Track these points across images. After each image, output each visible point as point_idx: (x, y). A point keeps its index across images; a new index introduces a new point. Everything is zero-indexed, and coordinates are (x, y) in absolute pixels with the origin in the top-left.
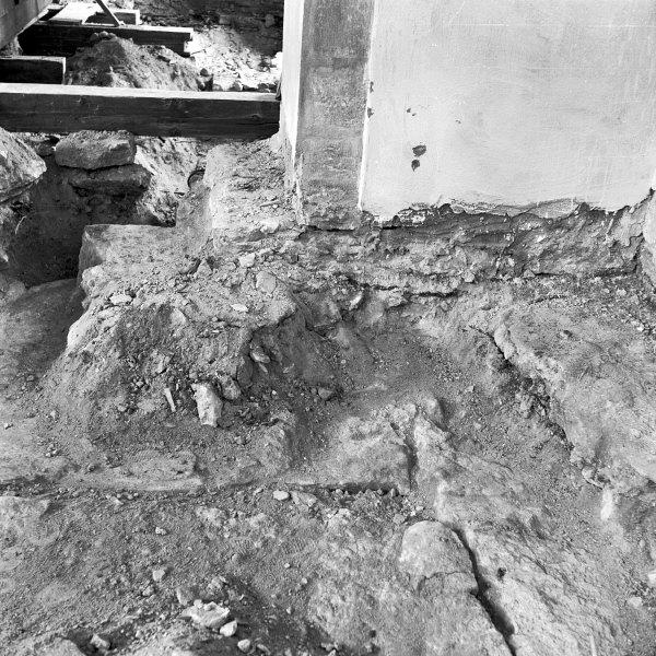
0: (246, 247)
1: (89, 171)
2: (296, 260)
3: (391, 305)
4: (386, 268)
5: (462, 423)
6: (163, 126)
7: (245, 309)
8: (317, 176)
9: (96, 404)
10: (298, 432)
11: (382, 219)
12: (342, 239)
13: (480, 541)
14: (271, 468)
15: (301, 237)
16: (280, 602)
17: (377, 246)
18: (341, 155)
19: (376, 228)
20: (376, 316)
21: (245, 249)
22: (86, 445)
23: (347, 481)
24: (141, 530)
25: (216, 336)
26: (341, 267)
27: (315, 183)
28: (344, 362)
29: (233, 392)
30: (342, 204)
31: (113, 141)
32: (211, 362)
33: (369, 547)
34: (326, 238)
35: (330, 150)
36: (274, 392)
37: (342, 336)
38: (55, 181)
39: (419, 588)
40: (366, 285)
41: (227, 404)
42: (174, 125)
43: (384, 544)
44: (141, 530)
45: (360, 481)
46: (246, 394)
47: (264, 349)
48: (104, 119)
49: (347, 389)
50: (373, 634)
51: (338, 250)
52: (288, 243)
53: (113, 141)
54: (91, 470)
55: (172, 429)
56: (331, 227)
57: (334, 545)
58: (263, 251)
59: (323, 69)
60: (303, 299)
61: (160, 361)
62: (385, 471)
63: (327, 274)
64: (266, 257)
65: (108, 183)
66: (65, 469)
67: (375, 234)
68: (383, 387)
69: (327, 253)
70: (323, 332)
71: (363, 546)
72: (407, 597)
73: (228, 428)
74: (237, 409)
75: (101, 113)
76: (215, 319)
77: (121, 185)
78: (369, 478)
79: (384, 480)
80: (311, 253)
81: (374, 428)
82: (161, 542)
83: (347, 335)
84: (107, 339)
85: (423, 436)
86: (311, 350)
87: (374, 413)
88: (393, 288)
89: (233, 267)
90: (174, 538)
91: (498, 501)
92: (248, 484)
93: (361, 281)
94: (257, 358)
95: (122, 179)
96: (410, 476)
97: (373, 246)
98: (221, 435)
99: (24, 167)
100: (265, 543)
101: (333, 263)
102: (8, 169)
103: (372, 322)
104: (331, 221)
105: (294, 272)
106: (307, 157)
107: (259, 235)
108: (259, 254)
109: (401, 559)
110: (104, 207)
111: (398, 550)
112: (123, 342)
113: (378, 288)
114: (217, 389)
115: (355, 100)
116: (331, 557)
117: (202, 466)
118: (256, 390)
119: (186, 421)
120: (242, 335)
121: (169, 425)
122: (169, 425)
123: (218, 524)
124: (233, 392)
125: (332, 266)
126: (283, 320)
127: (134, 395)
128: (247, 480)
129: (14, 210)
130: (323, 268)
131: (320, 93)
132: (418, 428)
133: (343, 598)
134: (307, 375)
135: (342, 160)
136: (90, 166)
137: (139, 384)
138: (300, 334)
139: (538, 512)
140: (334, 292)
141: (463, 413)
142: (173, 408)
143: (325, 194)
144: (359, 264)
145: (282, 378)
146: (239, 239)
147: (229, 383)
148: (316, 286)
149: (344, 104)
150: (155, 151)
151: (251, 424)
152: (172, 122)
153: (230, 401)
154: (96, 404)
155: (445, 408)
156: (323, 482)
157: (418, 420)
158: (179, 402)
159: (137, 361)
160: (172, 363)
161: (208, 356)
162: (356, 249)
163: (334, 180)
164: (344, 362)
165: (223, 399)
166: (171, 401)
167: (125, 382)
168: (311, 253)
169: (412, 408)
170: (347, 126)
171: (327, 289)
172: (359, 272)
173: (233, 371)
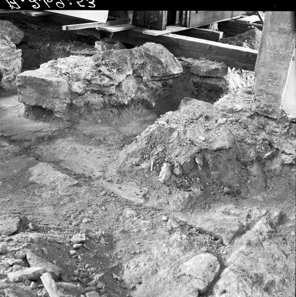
0: (225, 115)
1: (201, 77)
2: (246, 128)
3: (286, 162)
4: (291, 144)
5: (286, 229)
6: (240, 64)
7: (204, 139)
8: (262, 87)
9: (127, 158)
11: (290, 117)
12: (271, 122)
13: (228, 274)
14: (172, 207)
15: (251, 117)
16: (119, 253)
17: (288, 130)
18: (276, 79)
19: (287, 121)
20: (276, 165)
21: (224, 116)
22: (114, 172)
23: (200, 226)
24: (97, 205)
25: (184, 146)
26: (267, 137)
27: (261, 90)
28: (249, 181)
29: (177, 171)
30: (273, 104)
31: (215, 66)
32: (176, 156)
33: (177, 253)
34: (262, 120)
35: (271, 75)
36: (198, 179)
37: (254, 169)
38: (187, 78)
39: (178, 277)
40: (278, 149)
41: (174, 176)
42: (246, 64)
43: (184, 255)
44: (97, 205)
45: (206, 229)
46: (184, 174)
47: (204, 159)
48: (217, 56)
49: (243, 194)
50: (140, 283)
51: (267, 128)
52: (244, 118)
53: (215, 66)
54: (108, 181)
55: (145, 179)
56: (265, 115)
58: (231, 119)
59: (274, 33)
60: (241, 146)
61: (160, 149)
62: (222, 230)
63: (259, 138)
64: (232, 122)
65: (207, 84)
66: (100, 177)
67: (287, 124)
68: (261, 200)
69: (262, 128)
70: (245, 164)
72: (170, 278)
73: (168, 186)
74: (177, 179)
75: (216, 54)
76: (188, 139)
77: (212, 86)
78: (211, 229)
79: (218, 234)
80: (254, 125)
81: (237, 213)
82: (100, 212)
83: (257, 170)
84: (146, 135)
85: (261, 226)
87: (245, 208)
88: (291, 154)
89: (214, 122)
90: (106, 213)
91: (262, 266)
92: (159, 210)
93: (276, 146)
94: (197, 161)
95: (213, 83)
96: (234, 238)
97: (286, 130)
98: (164, 186)
99: (170, 68)
100: (139, 231)
101: (264, 133)
102: (163, 67)
103: (273, 167)
104: (265, 112)
105: (242, 133)
106: (259, 77)
107: (232, 111)
108: (229, 119)
109: (185, 264)
110: (203, 94)
111: (187, 260)
112: (150, 139)
113: (283, 152)
114: (172, 168)
115: (288, 51)
116: (159, 249)
117: (148, 196)
118: (191, 175)
119: (154, 177)
120: (195, 149)
121: (147, 176)
122: (147, 176)
123: (128, 217)
124: (177, 171)
125: (263, 135)
126: (219, 150)
127: (143, 159)
128: (159, 208)
129: (163, 85)
130: (258, 135)
131: (270, 45)
132: (260, 222)
134: (225, 180)
136: (201, 74)
137: (147, 156)
138: (229, 160)
139: (277, 279)
140: (257, 147)
141: (290, 224)
142: (151, 170)
143: (265, 97)
144: (277, 138)
145: (209, 176)
146: (223, 111)
147: (177, 167)
148: (249, 141)
149: (281, 53)
150: (247, 79)
151: (178, 188)
152: (244, 62)
153: (175, 175)
154: (127, 158)
155: (282, 218)
156: (190, 223)
157: (263, 218)
158: (155, 168)
159: (151, 147)
160: (162, 152)
161: (176, 154)
162: (277, 130)
163: (271, 91)
164: (249, 181)
165: (172, 172)
166: (152, 166)
167: (142, 154)
168: (254, 125)
169: (264, 212)
170: (281, 64)
171: (255, 144)
172: (276, 142)
173: (182, 163)
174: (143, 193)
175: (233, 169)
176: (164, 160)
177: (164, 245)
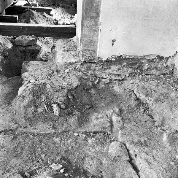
0: (67, 67)
1: (24, 47)
2: (80, 70)
3: (106, 83)
4: (105, 73)
5: (125, 115)
6: (44, 34)
7: (66, 84)
8: (86, 48)
9: (26, 110)
10: (81, 117)
11: (104, 59)
12: (93, 65)
13: (130, 147)
14: (74, 127)
15: (82, 64)
16: (76, 163)
17: (102, 67)
18: (93, 42)
19: (102, 62)
20: (102, 86)
21: (67, 68)
23: (94, 130)
24: (38, 144)
25: (59, 91)
26: (92, 73)
27: (86, 50)
28: (93, 98)
29: (63, 106)
30: (93, 55)
31: (31, 38)
32: (57, 98)
33: (100, 148)
34: (88, 65)
35: (90, 41)
36: (74, 106)
37: (93, 91)
38: (15, 49)
39: (114, 160)
40: (99, 77)
41: (62, 110)
42: (47, 34)
44: (38, 144)
45: (98, 130)
46: (67, 107)
47: (72, 95)
48: (28, 32)
49: (94, 106)
50: (101, 172)
51: (92, 68)
52: (78, 66)
53: (31, 38)
54: (25, 128)
55: (47, 116)
56: (90, 62)
58: (71, 68)
59: (88, 19)
60: (82, 81)
61: (43, 98)
62: (105, 128)
63: (89, 74)
64: (72, 70)
65: (29, 50)
66: (18, 127)
67: (102, 64)
68: (104, 105)
69: (89, 69)
70: (88, 90)
71: (99, 148)
72: (110, 162)
73: (62, 116)
74: (64, 111)
75: (28, 31)
76: (58, 87)
77: (33, 50)
78: (100, 130)
79: (104, 130)
80: (84, 69)
81: (102, 116)
82: (44, 147)
83: (94, 91)
85: (115, 118)
87: (101, 112)
88: (107, 78)
89: (63, 72)
91: (135, 136)
92: (67, 131)
93: (98, 76)
94: (70, 97)
95: (33, 49)
97: (101, 67)
98: (60, 118)
100: (72, 147)
101: (90, 71)
102: (2, 46)
103: (101, 87)
104: (90, 60)
105: (80, 74)
106: (83, 43)
107: (70, 64)
108: (70, 69)
109: (109, 152)
110: (28, 56)
111: (108, 149)
112: (34, 93)
113: (102, 78)
114: (59, 106)
115: (96, 27)
116: (90, 151)
117: (55, 127)
118: (70, 106)
119: (50, 114)
120: (66, 91)
121: (46, 115)
122: (46, 115)
123: (59, 142)
124: (63, 106)
125: (90, 72)
126: (77, 87)
127: (36, 107)
128: (67, 130)
129: (4, 57)
130: (88, 73)
131: (87, 25)
132: (113, 116)
135: (93, 43)
136: (24, 45)
137: (38, 104)
139: (146, 139)
140: (91, 79)
141: (126, 112)
142: (47, 111)
143: (88, 53)
144: (97, 72)
145: (77, 102)
146: (65, 65)
147: (62, 104)
148: (86, 78)
149: (93, 28)
150: (42, 41)
151: (68, 115)
152: (47, 33)
153: (63, 109)
154: (26, 110)
155: (121, 111)
156: (88, 131)
157: (113, 114)
158: (48, 109)
159: (37, 98)
160: (47, 98)
161: (57, 97)
162: (97, 68)
163: (91, 49)
164: (93, 98)
165: (61, 108)
166: (46, 109)
167: (34, 104)
168: (84, 69)
170: (94, 34)
171: (89, 78)
172: (97, 74)
173: (63, 101)
174: (52, 126)
175: (84, 95)
176: (51, 103)
177: (91, 148)
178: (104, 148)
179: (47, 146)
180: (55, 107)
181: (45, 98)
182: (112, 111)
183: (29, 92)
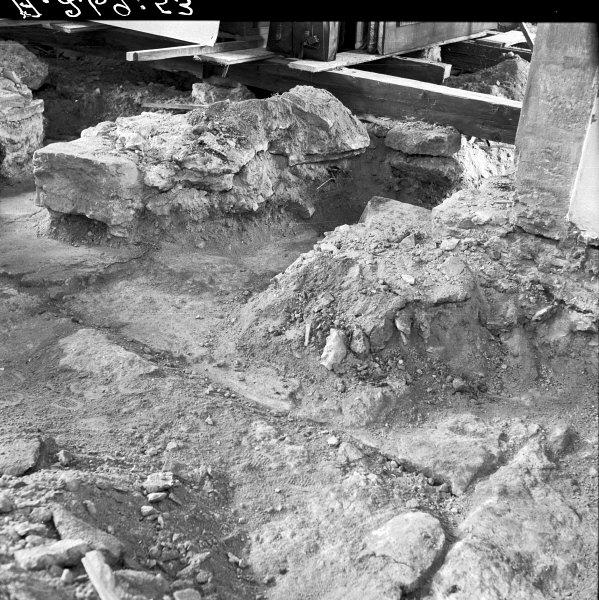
0: (455, 232)
1: (408, 155)
2: (497, 258)
3: (579, 328)
4: (589, 290)
5: (580, 462)
6: (486, 129)
7: (412, 281)
8: (531, 176)
9: (257, 320)
10: (399, 401)
11: (587, 235)
12: (548, 247)
13: (462, 554)
14: (348, 418)
15: (508, 236)
16: (241, 511)
17: (583, 263)
18: (558, 159)
19: (581, 244)
20: (558, 334)
21: (454, 234)
23: (405, 457)
24: (196, 414)
25: (372, 295)
26: (540, 276)
27: (528, 183)
28: (504, 367)
29: (359, 346)
30: (552, 210)
31: (434, 132)
32: (357, 316)
33: (359, 510)
34: (531, 242)
35: (548, 152)
36: (401, 362)
37: (515, 342)
38: (379, 158)
39: (361, 561)
40: (562, 302)
41: (351, 355)
42: (497, 130)
44: (196, 414)
45: (418, 462)
46: (372, 352)
47: (412, 321)
48: (439, 114)
49: (492, 391)
50: (284, 572)
51: (541, 258)
52: (495, 238)
53: (434, 132)
54: (219, 366)
55: (294, 361)
56: (537, 231)
57: (333, 495)
58: (467, 240)
59: (554, 67)
60: (488, 294)
61: (323, 301)
62: (448, 465)
63: (525, 278)
64: (469, 246)
65: (420, 169)
66: (202, 358)
67: (580, 250)
68: (527, 403)
69: (530, 258)
70: (496, 332)
71: (354, 507)
72: (344, 561)
73: (340, 375)
74: (357, 362)
75: (437, 108)
76: (381, 281)
77: (429, 173)
78: (428, 464)
79: (442, 472)
80: (514, 253)
82: (203, 428)
83: (521, 344)
85: (527, 456)
86: (472, 342)
87: (496, 419)
88: (588, 312)
89: (434, 246)
91: (531, 537)
92: (321, 424)
93: (558, 296)
94: (398, 326)
95: (431, 168)
97: (578, 264)
98: (332, 377)
100: (282, 467)
101: (534, 269)
102: (330, 136)
103: (552, 338)
104: (537, 226)
105: (489, 268)
106: (525, 155)
107: (470, 224)
108: (463, 241)
109: (374, 533)
110: (412, 190)
111: (378, 525)
112: (304, 280)
113: (573, 308)
114: (348, 339)
115: (582, 103)
116: (321, 502)
117: (299, 396)
118: (386, 353)
119: (311, 357)
120: (395, 302)
121: (297, 356)
122: (297, 356)
123: (259, 437)
124: (359, 346)
125: (533, 272)
126: (444, 303)
127: (290, 322)
128: (323, 421)
129: (329, 172)
130: (522, 272)
131: (546, 91)
132: (526, 448)
133: (293, 535)
135: (559, 164)
136: (407, 150)
137: (297, 316)
138: (464, 323)
140: (521, 297)
141: (587, 454)
142: (306, 343)
143: (535, 196)
144: (561, 278)
145: (422, 355)
146: (451, 223)
147: (359, 337)
148: (505, 286)
149: (569, 106)
150: (499, 159)
151: (360, 379)
152: (495, 126)
153: (355, 353)
154: (257, 320)
155: (571, 441)
156: (384, 450)
157: (531, 441)
158: (313, 339)
159: (306, 297)
160: (328, 306)
161: (357, 310)
162: (561, 262)
163: (548, 183)
164: (504, 367)
165: (349, 348)
166: (307, 336)
167: (288, 310)
168: (514, 253)
170: (569, 130)
171: (515, 292)
172: (558, 286)
173: (368, 329)
178: (372, 514)
179: (214, 430)
180: (333, 338)
181: (327, 302)
182: (534, 428)
183: (295, 272)
